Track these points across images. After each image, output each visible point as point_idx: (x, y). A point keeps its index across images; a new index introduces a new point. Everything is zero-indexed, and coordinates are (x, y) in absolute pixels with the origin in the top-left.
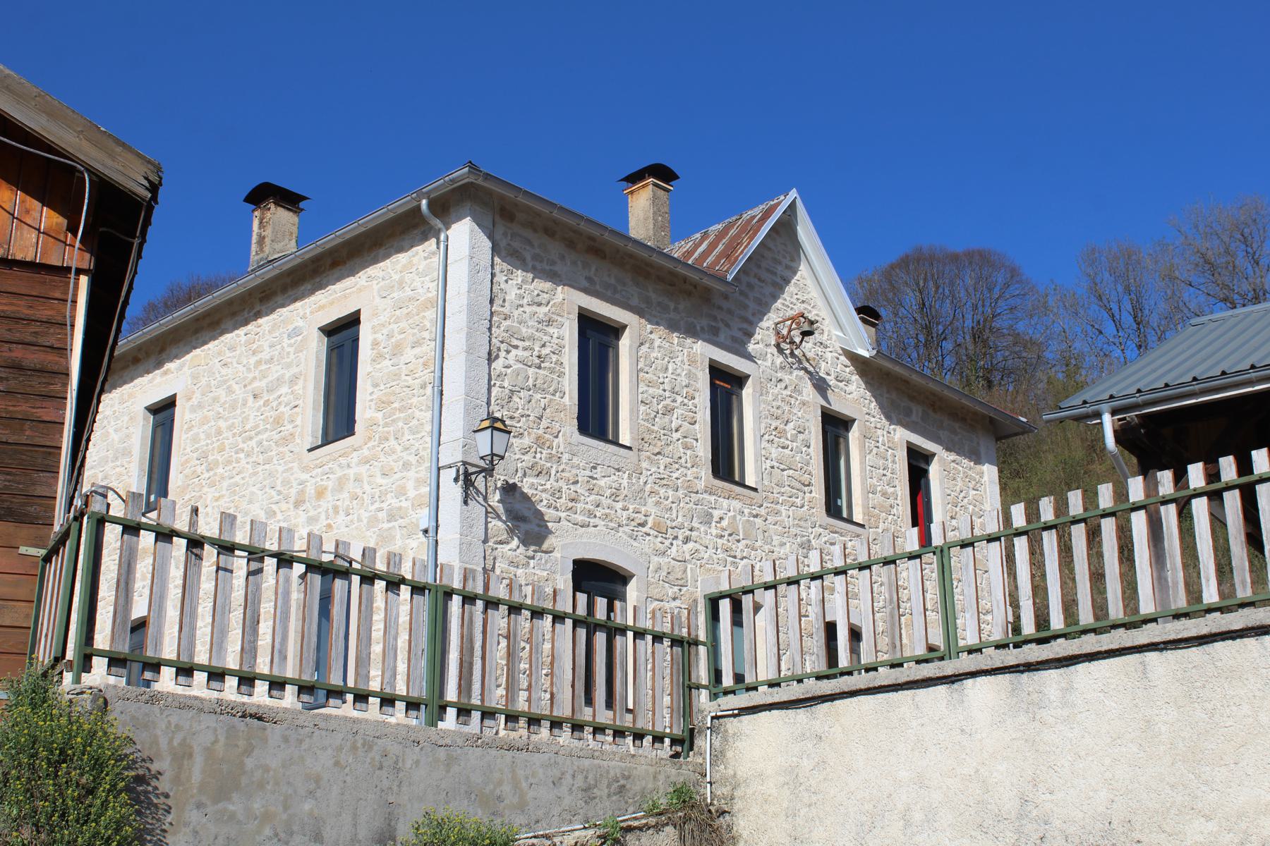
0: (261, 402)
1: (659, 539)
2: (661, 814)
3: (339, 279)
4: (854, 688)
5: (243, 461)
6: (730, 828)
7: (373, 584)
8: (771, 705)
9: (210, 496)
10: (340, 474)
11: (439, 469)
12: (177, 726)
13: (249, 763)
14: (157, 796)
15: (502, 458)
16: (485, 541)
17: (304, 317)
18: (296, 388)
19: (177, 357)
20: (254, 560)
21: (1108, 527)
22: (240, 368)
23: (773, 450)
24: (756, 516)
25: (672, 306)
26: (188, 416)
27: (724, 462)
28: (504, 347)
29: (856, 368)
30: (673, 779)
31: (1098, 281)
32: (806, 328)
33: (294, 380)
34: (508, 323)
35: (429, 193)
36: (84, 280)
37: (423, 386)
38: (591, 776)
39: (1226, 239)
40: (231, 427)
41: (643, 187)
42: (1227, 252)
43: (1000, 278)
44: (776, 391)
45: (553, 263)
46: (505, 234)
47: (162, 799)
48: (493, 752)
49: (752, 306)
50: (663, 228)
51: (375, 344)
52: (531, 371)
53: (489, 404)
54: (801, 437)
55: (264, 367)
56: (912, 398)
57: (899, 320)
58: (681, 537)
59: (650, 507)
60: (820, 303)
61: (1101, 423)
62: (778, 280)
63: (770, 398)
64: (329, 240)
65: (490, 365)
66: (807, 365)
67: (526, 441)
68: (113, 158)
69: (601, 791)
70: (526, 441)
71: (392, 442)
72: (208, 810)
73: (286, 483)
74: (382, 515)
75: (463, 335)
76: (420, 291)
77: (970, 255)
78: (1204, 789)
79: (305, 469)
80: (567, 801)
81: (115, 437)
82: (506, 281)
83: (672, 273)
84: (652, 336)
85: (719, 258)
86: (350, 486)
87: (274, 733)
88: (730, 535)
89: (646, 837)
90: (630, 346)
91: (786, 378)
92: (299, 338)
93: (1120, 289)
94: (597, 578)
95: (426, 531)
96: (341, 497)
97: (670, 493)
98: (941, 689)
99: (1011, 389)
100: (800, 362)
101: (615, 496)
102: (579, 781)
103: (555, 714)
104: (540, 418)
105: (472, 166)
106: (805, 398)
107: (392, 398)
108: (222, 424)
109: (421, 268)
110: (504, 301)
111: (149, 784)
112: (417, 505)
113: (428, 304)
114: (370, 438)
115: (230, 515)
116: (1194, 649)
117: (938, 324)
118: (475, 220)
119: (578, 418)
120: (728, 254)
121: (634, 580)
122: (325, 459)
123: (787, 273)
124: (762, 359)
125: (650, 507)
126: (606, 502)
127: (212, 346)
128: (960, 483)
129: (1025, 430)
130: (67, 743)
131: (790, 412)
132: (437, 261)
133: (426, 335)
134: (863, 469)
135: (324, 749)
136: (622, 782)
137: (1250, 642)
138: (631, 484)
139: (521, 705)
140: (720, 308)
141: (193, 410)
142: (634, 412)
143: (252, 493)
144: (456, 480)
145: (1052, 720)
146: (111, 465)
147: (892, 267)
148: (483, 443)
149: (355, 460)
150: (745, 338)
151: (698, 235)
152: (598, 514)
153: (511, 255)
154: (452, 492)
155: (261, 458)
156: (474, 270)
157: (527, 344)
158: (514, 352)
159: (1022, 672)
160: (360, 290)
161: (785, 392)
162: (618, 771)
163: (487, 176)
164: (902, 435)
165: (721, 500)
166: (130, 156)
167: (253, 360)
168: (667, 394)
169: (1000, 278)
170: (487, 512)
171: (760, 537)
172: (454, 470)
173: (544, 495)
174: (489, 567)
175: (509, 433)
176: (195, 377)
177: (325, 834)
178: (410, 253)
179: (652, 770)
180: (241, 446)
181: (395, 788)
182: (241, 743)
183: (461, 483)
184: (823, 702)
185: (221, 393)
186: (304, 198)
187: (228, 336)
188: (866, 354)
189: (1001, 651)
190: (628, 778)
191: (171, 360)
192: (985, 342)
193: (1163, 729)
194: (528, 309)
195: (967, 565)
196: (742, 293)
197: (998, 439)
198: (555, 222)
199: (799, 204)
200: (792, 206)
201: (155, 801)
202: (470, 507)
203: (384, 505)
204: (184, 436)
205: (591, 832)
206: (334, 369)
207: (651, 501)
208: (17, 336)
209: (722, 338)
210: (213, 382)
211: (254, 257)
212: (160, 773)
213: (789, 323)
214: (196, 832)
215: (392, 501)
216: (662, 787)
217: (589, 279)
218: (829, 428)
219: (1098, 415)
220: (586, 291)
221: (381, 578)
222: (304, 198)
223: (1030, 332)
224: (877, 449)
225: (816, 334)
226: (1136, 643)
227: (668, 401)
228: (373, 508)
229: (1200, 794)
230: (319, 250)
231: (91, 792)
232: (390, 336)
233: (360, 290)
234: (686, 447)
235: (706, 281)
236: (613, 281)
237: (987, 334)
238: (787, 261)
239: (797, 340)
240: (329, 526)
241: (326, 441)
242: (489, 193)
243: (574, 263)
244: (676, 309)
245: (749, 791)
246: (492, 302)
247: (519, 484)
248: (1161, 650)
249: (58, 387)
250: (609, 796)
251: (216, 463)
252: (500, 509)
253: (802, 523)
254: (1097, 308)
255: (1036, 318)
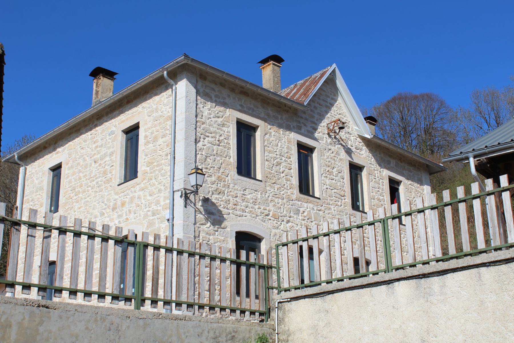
0: (98, 165)
1: (275, 222)
3: (130, 109)
4: (343, 287)
5: (91, 191)
8: (305, 296)
9: (76, 207)
10: (131, 195)
11: (174, 192)
13: (41, 329)
15: (201, 186)
16: (195, 224)
17: (115, 126)
18: (112, 158)
19: (62, 146)
20: (46, 231)
22: (89, 149)
23: (327, 181)
24: (320, 210)
25: (280, 117)
26: (67, 172)
27: (305, 187)
28: (202, 136)
29: (365, 143)
30: (259, 332)
31: (479, 105)
32: (341, 125)
34: (204, 126)
35: (167, 69)
37: (167, 155)
38: (217, 332)
40: (85, 176)
41: (268, 65)
43: (436, 105)
44: (328, 154)
45: (225, 99)
46: (202, 86)
49: (316, 116)
50: (277, 83)
51: (146, 137)
53: (196, 162)
54: (340, 174)
55: (99, 149)
56: (390, 156)
57: (392, 125)
58: (285, 221)
60: (348, 114)
61: (469, 162)
62: (328, 105)
63: (325, 157)
65: (196, 145)
66: (342, 142)
67: (213, 179)
70: (213, 179)
71: (154, 181)
73: (109, 200)
74: (150, 213)
75: (184, 131)
76: (165, 112)
77: (422, 96)
78: (510, 334)
79: (117, 194)
81: (36, 182)
82: (203, 107)
83: (279, 102)
84: (271, 131)
85: (301, 95)
86: (136, 201)
87: (54, 314)
88: (308, 219)
90: (261, 135)
91: (333, 148)
92: (114, 135)
93: (489, 109)
95: (168, 220)
96: (132, 206)
97: (280, 201)
98: (384, 287)
99: (442, 154)
101: (254, 203)
102: (211, 334)
103: (200, 302)
104: (220, 168)
105: (186, 56)
106: (342, 157)
107: (154, 161)
108: (81, 175)
109: (165, 102)
110: (202, 116)
112: (164, 209)
113: (169, 118)
114: (144, 179)
115: (34, 210)
116: (503, 265)
117: (409, 126)
119: (237, 168)
120: (305, 94)
121: (264, 240)
122: (125, 189)
123: (332, 102)
125: (271, 207)
126: (250, 205)
127: (77, 140)
128: (413, 194)
129: (443, 170)
131: (335, 164)
132: (172, 99)
133: (168, 132)
134: (369, 189)
135: (80, 321)
136: (233, 334)
138: (262, 197)
140: (301, 117)
141: (69, 169)
142: (263, 164)
143: (94, 205)
144: (181, 196)
146: (35, 194)
147: (389, 102)
148: (192, 180)
149: (138, 189)
150: (313, 131)
151: (293, 86)
152: (247, 211)
153: (205, 95)
154: (179, 202)
155: (98, 190)
156: (188, 103)
157: (213, 135)
158: (207, 139)
159: (421, 278)
160: (139, 113)
161: (332, 155)
162: (231, 329)
163: (193, 60)
164: (386, 173)
165: (303, 203)
167: (94, 146)
169: (436, 105)
170: (195, 211)
171: (322, 220)
172: (180, 192)
173: (222, 203)
174: (197, 235)
175: (204, 175)
176: (70, 155)
178: (160, 96)
179: (248, 328)
180: (89, 184)
181: (117, 340)
182: (37, 320)
183: (183, 198)
184: (329, 294)
185: (81, 161)
186: (117, 74)
187: (84, 135)
188: (369, 137)
189: (412, 268)
191: (59, 147)
192: (430, 133)
193: (489, 305)
194: (213, 119)
195: (396, 227)
196: (312, 111)
197: (430, 174)
200: (334, 71)
202: (187, 209)
203: (151, 209)
204: (65, 181)
206: (129, 148)
209: (303, 131)
210: (77, 156)
211: (94, 100)
213: (333, 123)
215: (154, 207)
216: (253, 336)
217: (241, 106)
218: (352, 170)
219: (467, 158)
220: (240, 111)
221: (112, 239)
222: (117, 74)
223: (450, 129)
224: (376, 179)
225: (346, 128)
226: (476, 263)
227: (278, 160)
228: (145, 210)
229: (507, 337)
230: (121, 96)
233: (139, 113)
235: (294, 105)
236: (252, 106)
237: (431, 130)
238: (332, 96)
239: (337, 131)
241: (126, 181)
242: (195, 68)
243: (234, 98)
244: (281, 118)
245: (295, 337)
246: (196, 116)
247: (210, 198)
248: (488, 266)
250: (226, 341)
251: (79, 192)
252: (202, 209)
254: (479, 117)
255: (452, 123)
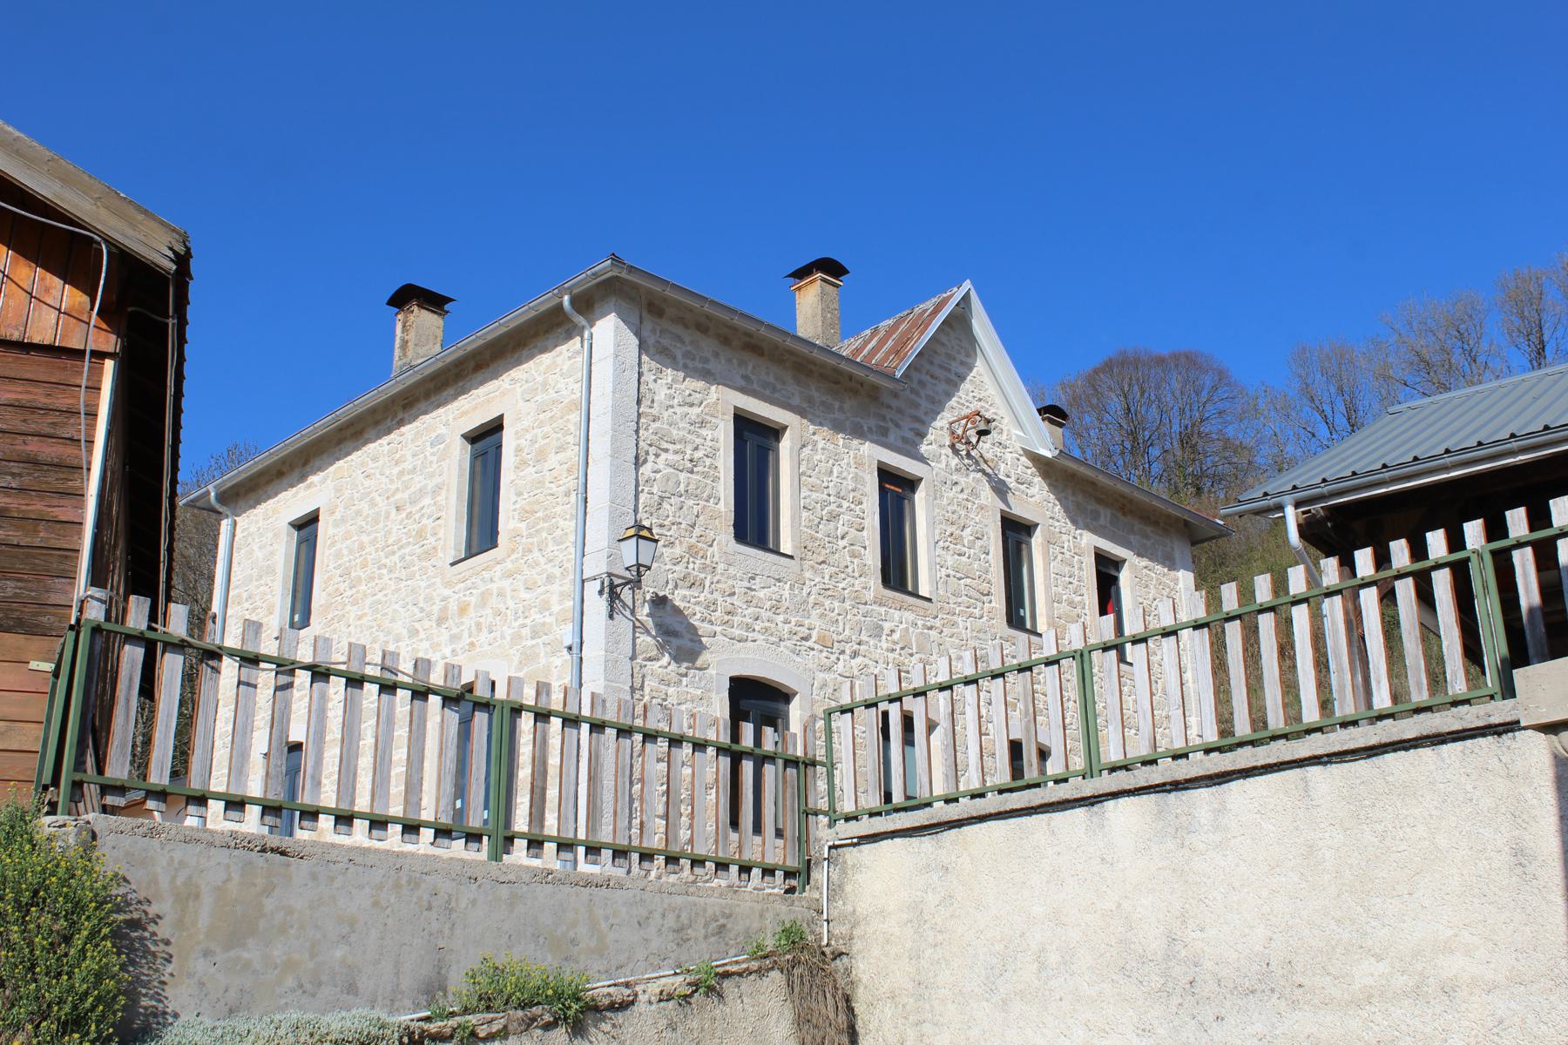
2: (766, 957)
3: (482, 383)
5: (386, 578)
6: (848, 972)
7: (426, 699)
10: (483, 588)
12: (181, 863)
13: (269, 904)
14: (156, 943)
16: (633, 658)
19: (320, 469)
20: (282, 673)
21: (1266, 622)
22: (384, 479)
24: (930, 628)
25: (837, 405)
26: (331, 531)
27: (896, 570)
28: (652, 450)
29: (1039, 470)
30: (782, 917)
32: (982, 427)
33: (436, 491)
34: (657, 424)
36: (109, 365)
37: (567, 494)
38: (683, 915)
39: (1441, 336)
42: (1443, 348)
43: (1208, 380)
44: (951, 494)
45: (706, 361)
46: (653, 331)
47: (162, 947)
48: (567, 889)
49: (924, 404)
51: (519, 450)
52: (683, 476)
53: (636, 511)
54: (979, 543)
55: (407, 477)
56: (1099, 501)
59: (814, 620)
60: (999, 401)
63: (945, 502)
64: (472, 341)
65: (637, 470)
66: (985, 467)
67: (678, 550)
68: (133, 226)
69: (697, 932)
70: (678, 550)
71: (536, 554)
72: (217, 959)
73: (429, 599)
74: (526, 632)
75: (608, 438)
77: (1176, 357)
79: (448, 584)
80: (655, 944)
81: (259, 554)
86: (494, 601)
89: (746, 984)
91: (962, 480)
93: (1333, 390)
94: (756, 699)
95: (570, 648)
97: (836, 604)
98: (1080, 812)
100: (979, 464)
101: (775, 609)
102: (670, 921)
104: (693, 526)
105: (615, 259)
107: (536, 507)
108: (365, 539)
111: (145, 929)
118: (620, 316)
119: (735, 526)
120: (898, 351)
124: (934, 462)
125: (814, 620)
126: (765, 614)
128: (1153, 591)
129: (1222, 533)
130: (42, 885)
132: (581, 360)
133: (570, 439)
134: (1047, 577)
135: (361, 887)
136: (722, 921)
137: (1425, 753)
138: (793, 596)
139: (605, 835)
140: (889, 407)
141: (336, 524)
142: (796, 518)
143: (395, 611)
144: (601, 592)
145: (1202, 846)
147: (1096, 371)
149: (498, 574)
150: (917, 439)
154: (597, 605)
156: (620, 370)
157: (678, 447)
158: (664, 456)
159: (1169, 791)
160: (503, 394)
163: (631, 269)
164: (1089, 541)
166: (153, 224)
167: (396, 470)
168: (832, 499)
169: (1208, 380)
170: (635, 627)
171: (935, 651)
172: (598, 582)
173: (697, 608)
174: (637, 685)
175: (656, 541)
176: (338, 490)
177: (360, 985)
178: (554, 353)
179: (758, 907)
181: (447, 931)
182: (260, 881)
183: (606, 595)
185: (364, 506)
187: (371, 446)
188: (1047, 454)
189: (1148, 768)
190: (729, 916)
194: (679, 410)
196: (913, 391)
197: (1193, 544)
198: (708, 317)
199: (973, 294)
200: (966, 298)
201: (153, 948)
203: (528, 621)
204: (327, 552)
205: (680, 979)
206: (478, 478)
207: (815, 613)
208: (33, 427)
209: (891, 438)
211: (397, 362)
212: (159, 917)
214: (202, 984)
217: (745, 377)
219: (1280, 508)
224: (1064, 553)
226: (1297, 756)
227: (833, 507)
230: (461, 353)
231: (67, 939)
232: (533, 441)
234: (853, 555)
235: (872, 378)
236: (771, 379)
237: (1195, 439)
239: (974, 440)
240: (472, 644)
242: (635, 287)
243: (729, 361)
244: (841, 409)
246: (639, 402)
248: (1325, 764)
249: (77, 484)
250: (706, 937)
251: (359, 580)
252: (650, 623)
253: (981, 635)
